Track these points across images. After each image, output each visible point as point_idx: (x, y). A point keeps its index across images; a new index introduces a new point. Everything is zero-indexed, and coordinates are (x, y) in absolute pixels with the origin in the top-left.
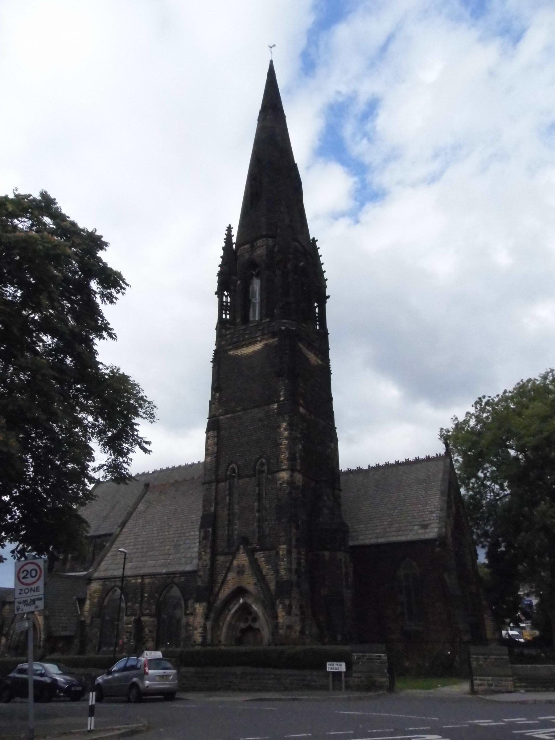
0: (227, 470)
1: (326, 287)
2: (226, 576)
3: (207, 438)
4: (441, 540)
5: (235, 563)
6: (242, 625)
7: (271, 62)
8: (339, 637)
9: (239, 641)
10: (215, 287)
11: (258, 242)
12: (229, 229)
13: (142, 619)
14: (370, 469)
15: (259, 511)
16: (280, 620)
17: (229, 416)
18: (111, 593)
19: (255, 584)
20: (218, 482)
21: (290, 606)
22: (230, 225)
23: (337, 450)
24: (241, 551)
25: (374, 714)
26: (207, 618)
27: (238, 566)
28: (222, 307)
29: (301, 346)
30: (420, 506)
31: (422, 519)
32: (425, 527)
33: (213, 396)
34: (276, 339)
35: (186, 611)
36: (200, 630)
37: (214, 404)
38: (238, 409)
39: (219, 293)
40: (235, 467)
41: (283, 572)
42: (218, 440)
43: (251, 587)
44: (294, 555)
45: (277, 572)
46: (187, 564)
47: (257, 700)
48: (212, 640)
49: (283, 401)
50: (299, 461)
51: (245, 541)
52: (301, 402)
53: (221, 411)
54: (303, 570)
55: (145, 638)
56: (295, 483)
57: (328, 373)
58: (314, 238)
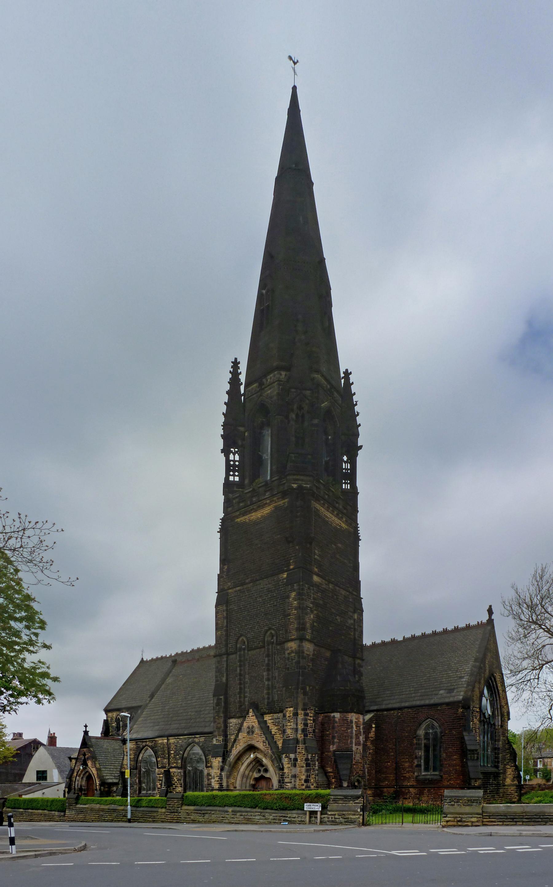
0: (237, 643)
1: (358, 435)
2: (237, 735)
3: (217, 613)
5: (245, 724)
6: (256, 775)
7: (294, 88)
8: (345, 784)
9: (254, 787)
10: (220, 443)
11: (269, 377)
12: (236, 364)
13: (171, 770)
15: (268, 680)
16: (286, 771)
17: (238, 588)
18: (143, 751)
19: (264, 742)
20: (228, 654)
21: (296, 760)
22: (236, 359)
24: (251, 714)
26: (222, 769)
27: (248, 727)
29: (318, 506)
30: (450, 672)
31: (449, 684)
33: (221, 569)
34: (286, 500)
35: (206, 765)
36: (217, 779)
37: (223, 577)
38: (247, 581)
39: (226, 451)
40: (245, 639)
41: (289, 731)
42: (227, 614)
43: (260, 745)
44: (301, 717)
45: (284, 732)
46: (206, 726)
47: (233, 831)
48: (228, 786)
49: (293, 569)
50: (309, 631)
51: (256, 707)
52: (316, 570)
53: (229, 584)
54: (311, 730)
55: (174, 784)
56: (303, 652)
57: (354, 538)
58: (347, 370)
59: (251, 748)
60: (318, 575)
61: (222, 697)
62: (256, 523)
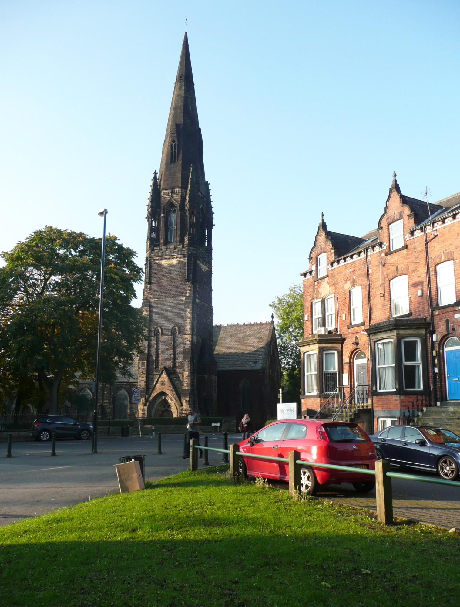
4: (263, 370)
5: (160, 379)
7: (186, 33)
10: (146, 214)
14: (228, 326)
23: (212, 319)
25: (281, 395)
27: (162, 381)
28: (151, 230)
32: (255, 363)
57: (210, 273)
59: (162, 393)
60: (198, 299)
61: (145, 362)
62: (168, 266)
